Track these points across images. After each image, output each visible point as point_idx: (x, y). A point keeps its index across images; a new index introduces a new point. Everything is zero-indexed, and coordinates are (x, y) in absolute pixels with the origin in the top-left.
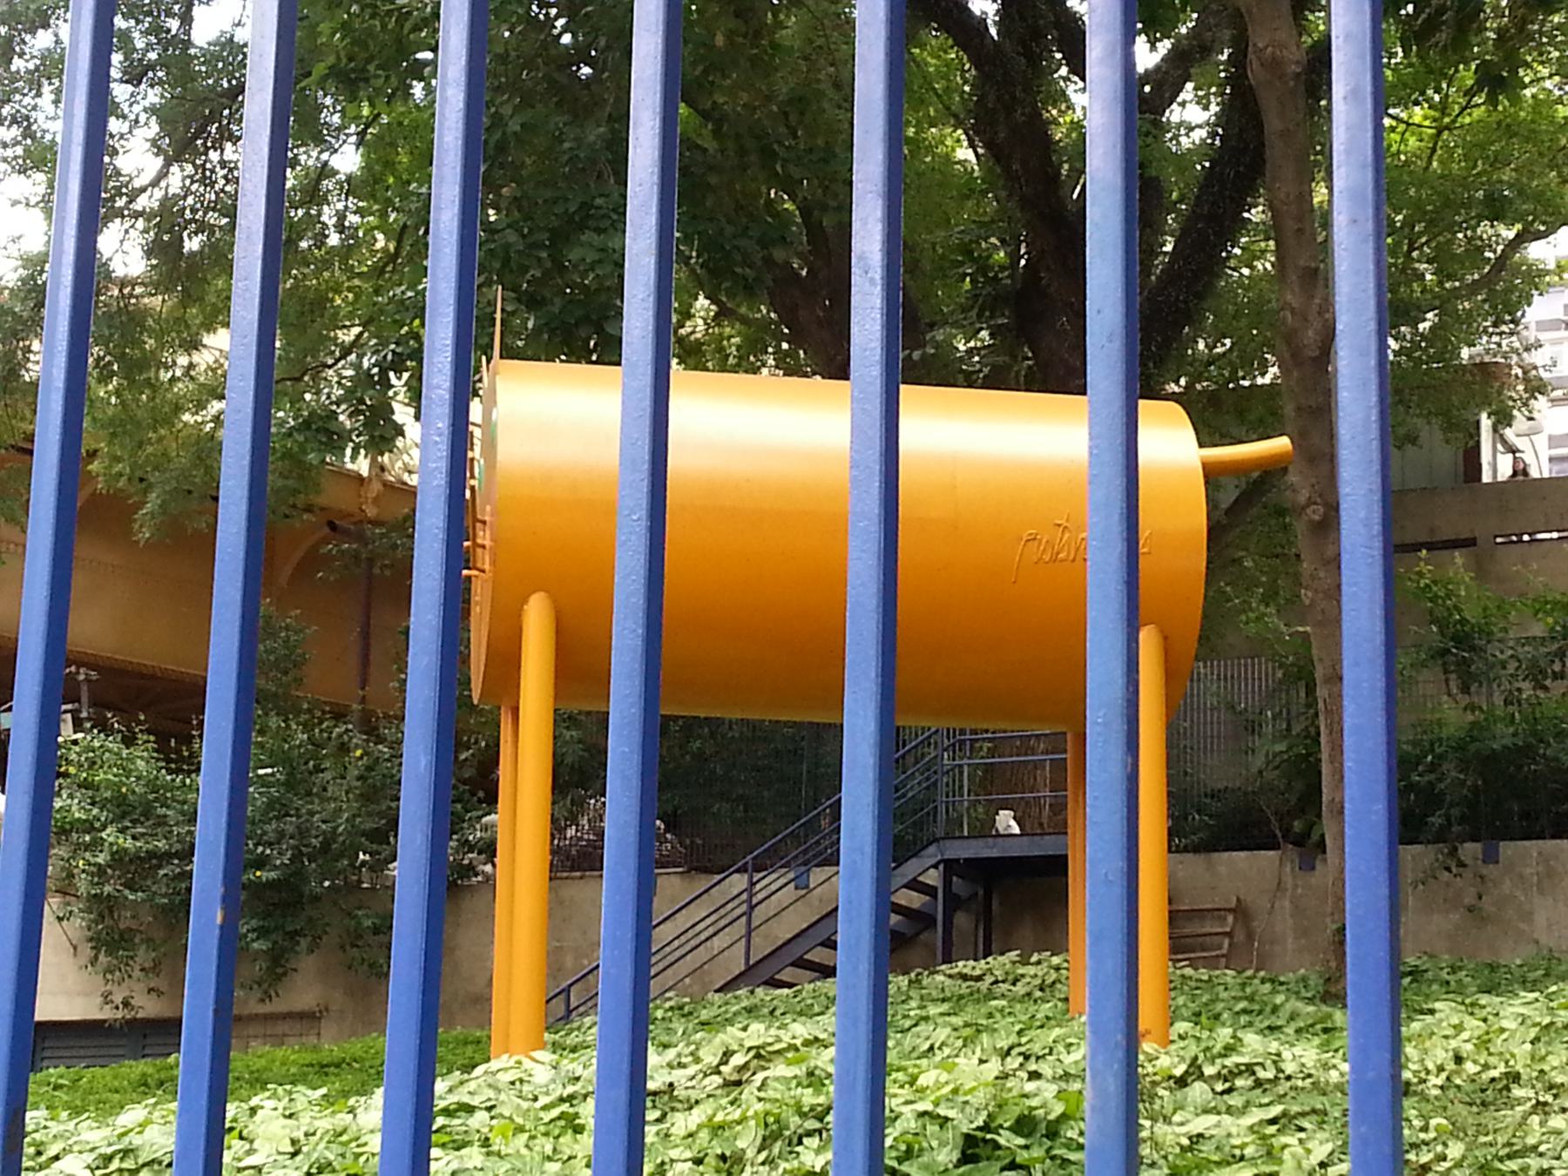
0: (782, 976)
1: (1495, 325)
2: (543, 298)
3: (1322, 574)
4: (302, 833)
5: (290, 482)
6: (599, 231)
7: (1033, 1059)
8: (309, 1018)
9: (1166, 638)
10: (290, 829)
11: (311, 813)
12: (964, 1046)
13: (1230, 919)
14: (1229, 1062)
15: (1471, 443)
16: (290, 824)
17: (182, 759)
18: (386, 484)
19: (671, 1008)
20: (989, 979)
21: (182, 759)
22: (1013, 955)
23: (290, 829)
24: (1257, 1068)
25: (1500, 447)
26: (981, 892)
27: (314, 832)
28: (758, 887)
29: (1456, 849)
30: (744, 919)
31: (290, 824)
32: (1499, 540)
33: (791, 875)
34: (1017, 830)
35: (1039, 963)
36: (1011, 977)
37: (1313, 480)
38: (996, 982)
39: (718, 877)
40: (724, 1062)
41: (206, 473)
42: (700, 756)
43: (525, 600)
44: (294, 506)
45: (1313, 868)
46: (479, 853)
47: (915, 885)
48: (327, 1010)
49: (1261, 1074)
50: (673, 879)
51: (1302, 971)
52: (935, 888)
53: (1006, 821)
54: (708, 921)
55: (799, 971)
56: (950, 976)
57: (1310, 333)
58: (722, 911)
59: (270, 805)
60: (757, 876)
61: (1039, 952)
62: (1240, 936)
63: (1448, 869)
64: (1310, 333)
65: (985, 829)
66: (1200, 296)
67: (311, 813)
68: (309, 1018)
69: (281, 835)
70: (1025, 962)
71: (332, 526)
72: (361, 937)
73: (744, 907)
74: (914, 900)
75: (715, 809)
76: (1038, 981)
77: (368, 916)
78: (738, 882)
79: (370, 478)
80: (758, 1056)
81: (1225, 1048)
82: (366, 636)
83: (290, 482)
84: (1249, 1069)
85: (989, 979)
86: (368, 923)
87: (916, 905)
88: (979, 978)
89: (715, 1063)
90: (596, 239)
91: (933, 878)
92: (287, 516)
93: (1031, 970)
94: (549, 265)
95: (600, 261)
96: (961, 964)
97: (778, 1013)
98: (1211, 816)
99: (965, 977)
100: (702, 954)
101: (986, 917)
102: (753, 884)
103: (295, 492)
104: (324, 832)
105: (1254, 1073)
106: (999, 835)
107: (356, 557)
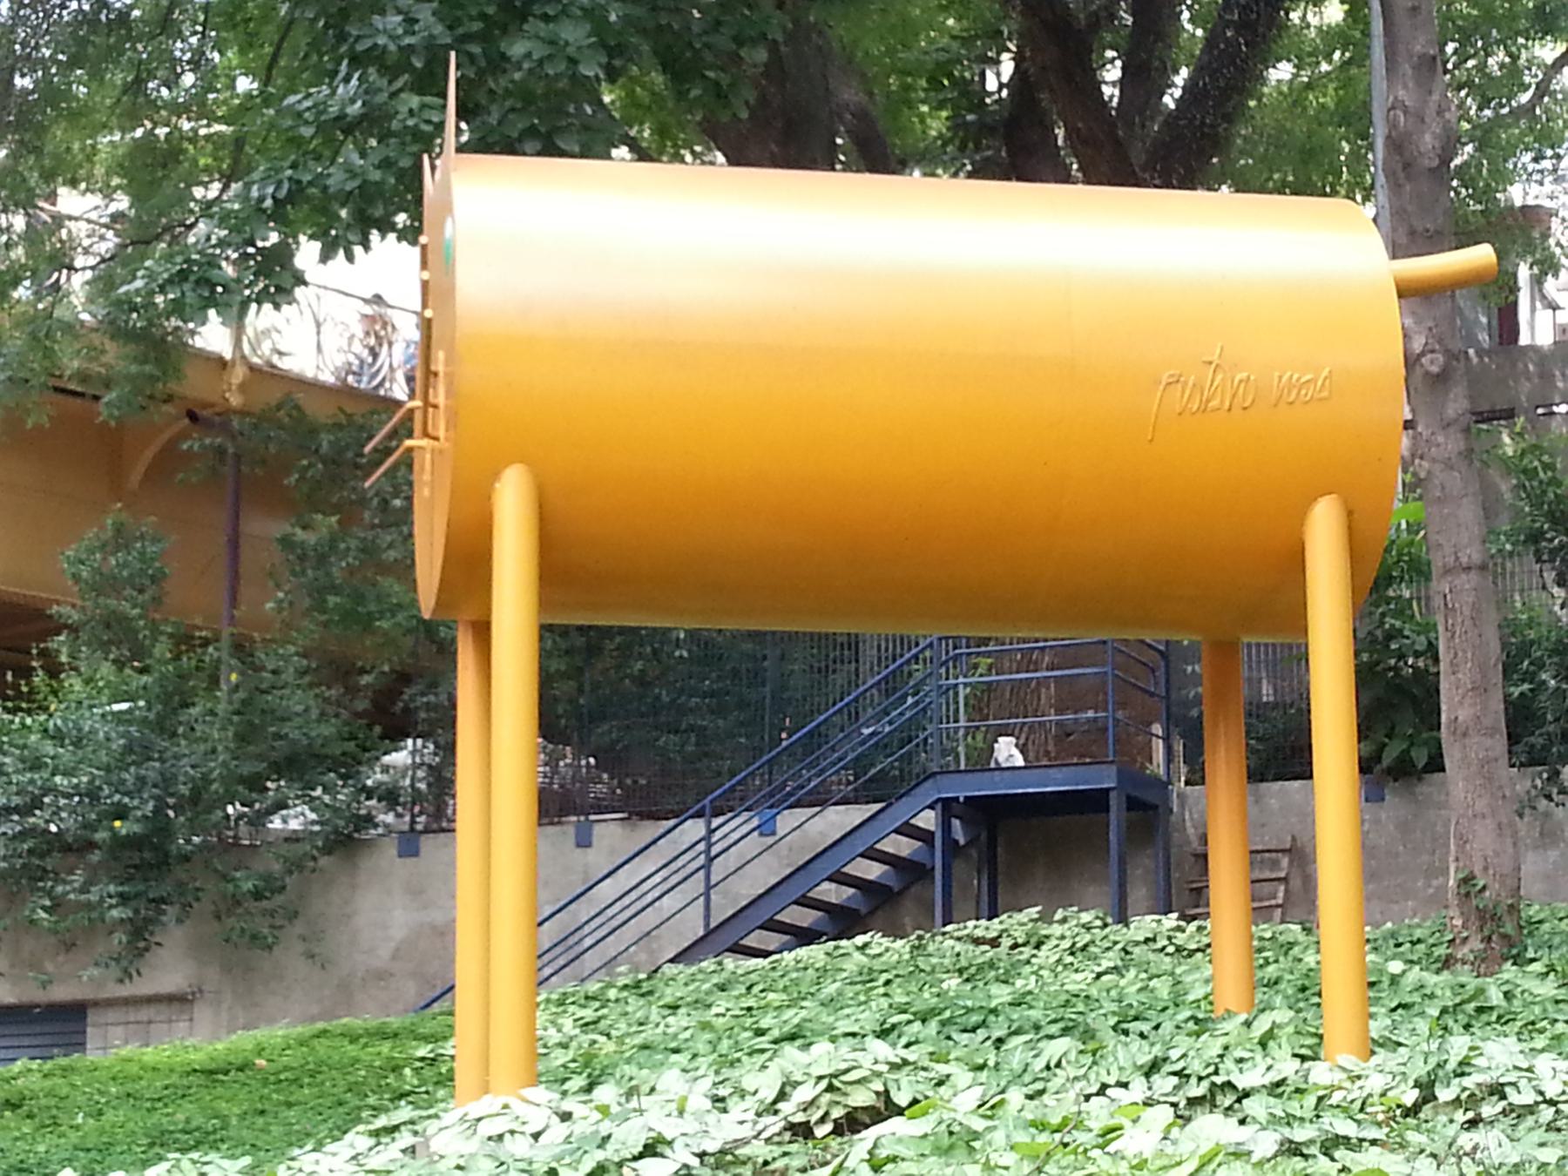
0: (750, 941)
1: (1536, 160)
2: (477, 105)
3: (1441, 439)
4: (167, 781)
5: (148, 368)
6: (546, 18)
7: (1193, 1080)
8: (179, 1001)
9: (1350, 513)
10: (152, 775)
11: (177, 757)
12: (1095, 1063)
13: (1285, 861)
14: (1468, 1082)
15: (1511, 298)
16: (152, 770)
17: (19, 696)
18: (252, 368)
19: (626, 987)
20: (1006, 942)
21: (19, 696)
22: (1033, 912)
23: (152, 775)
24: (1508, 1089)
25: (1538, 304)
26: (984, 836)
27: (182, 778)
28: (718, 835)
29: (1558, 773)
30: (702, 872)
31: (152, 770)
32: (1540, 411)
33: (755, 822)
34: (1019, 761)
35: (1064, 920)
36: (1034, 940)
37: (1431, 324)
38: (1015, 946)
39: (672, 822)
40: (782, 1096)
41: (45, 357)
42: (642, 681)
43: (496, 475)
44: (151, 397)
45: (1383, 799)
46: (379, 800)
47: (908, 830)
48: (201, 991)
49: (1514, 1098)
50: (613, 826)
51: (1389, 925)
52: (932, 833)
53: (1007, 751)
54: (657, 878)
55: (765, 933)
56: (959, 939)
57: (1428, 137)
58: (674, 866)
59: (128, 749)
60: (716, 822)
61: (1064, 908)
62: (1296, 883)
63: (1549, 797)
64: (1428, 137)
65: (982, 761)
66: (1229, 119)
67: (177, 757)
68: (179, 1001)
69: (141, 781)
70: (1045, 918)
71: (192, 416)
72: (239, 903)
73: (702, 859)
74: (903, 846)
75: (661, 743)
76: (1066, 944)
77: (248, 878)
78: (693, 829)
79: (233, 360)
80: (831, 1088)
81: (1461, 1064)
82: (234, 544)
83: (148, 368)
84: (1498, 1090)
85: (1006, 942)
86: (248, 886)
87: (905, 853)
88: (994, 943)
89: (770, 1100)
90: (542, 28)
91: (928, 820)
92: (143, 408)
93: (1057, 930)
94: (483, 64)
95: (550, 57)
96: (971, 924)
97: (756, 990)
98: (1258, 739)
99: (978, 941)
100: (650, 918)
101: (990, 865)
102: (712, 832)
103: (153, 379)
104: (193, 779)
105: (1503, 1097)
106: (999, 769)
107: (221, 452)
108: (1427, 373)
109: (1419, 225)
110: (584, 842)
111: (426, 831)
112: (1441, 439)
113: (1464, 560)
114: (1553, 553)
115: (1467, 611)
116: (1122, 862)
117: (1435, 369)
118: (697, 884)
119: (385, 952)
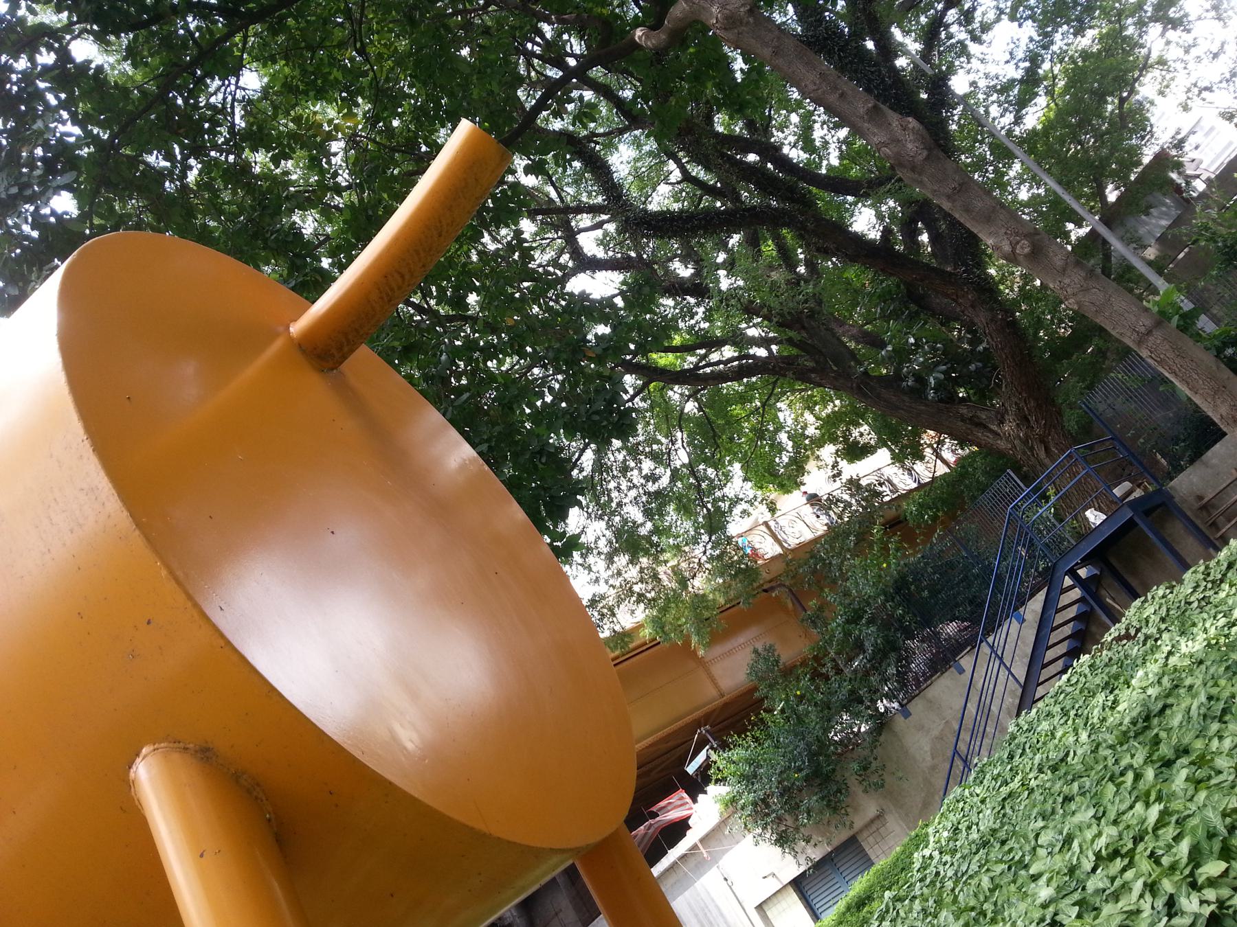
3: (1067, 281)
37: (1003, 231)
64: (910, 146)
65: (1085, 532)
73: (997, 662)
108: (1025, 256)
109: (948, 191)
110: (961, 671)
111: (909, 701)
112: (1067, 281)
113: (1143, 330)
114: (185, 46)
115: (1170, 355)
116: (1163, 540)
117: (1027, 250)
118: (1003, 673)
119: (929, 758)
